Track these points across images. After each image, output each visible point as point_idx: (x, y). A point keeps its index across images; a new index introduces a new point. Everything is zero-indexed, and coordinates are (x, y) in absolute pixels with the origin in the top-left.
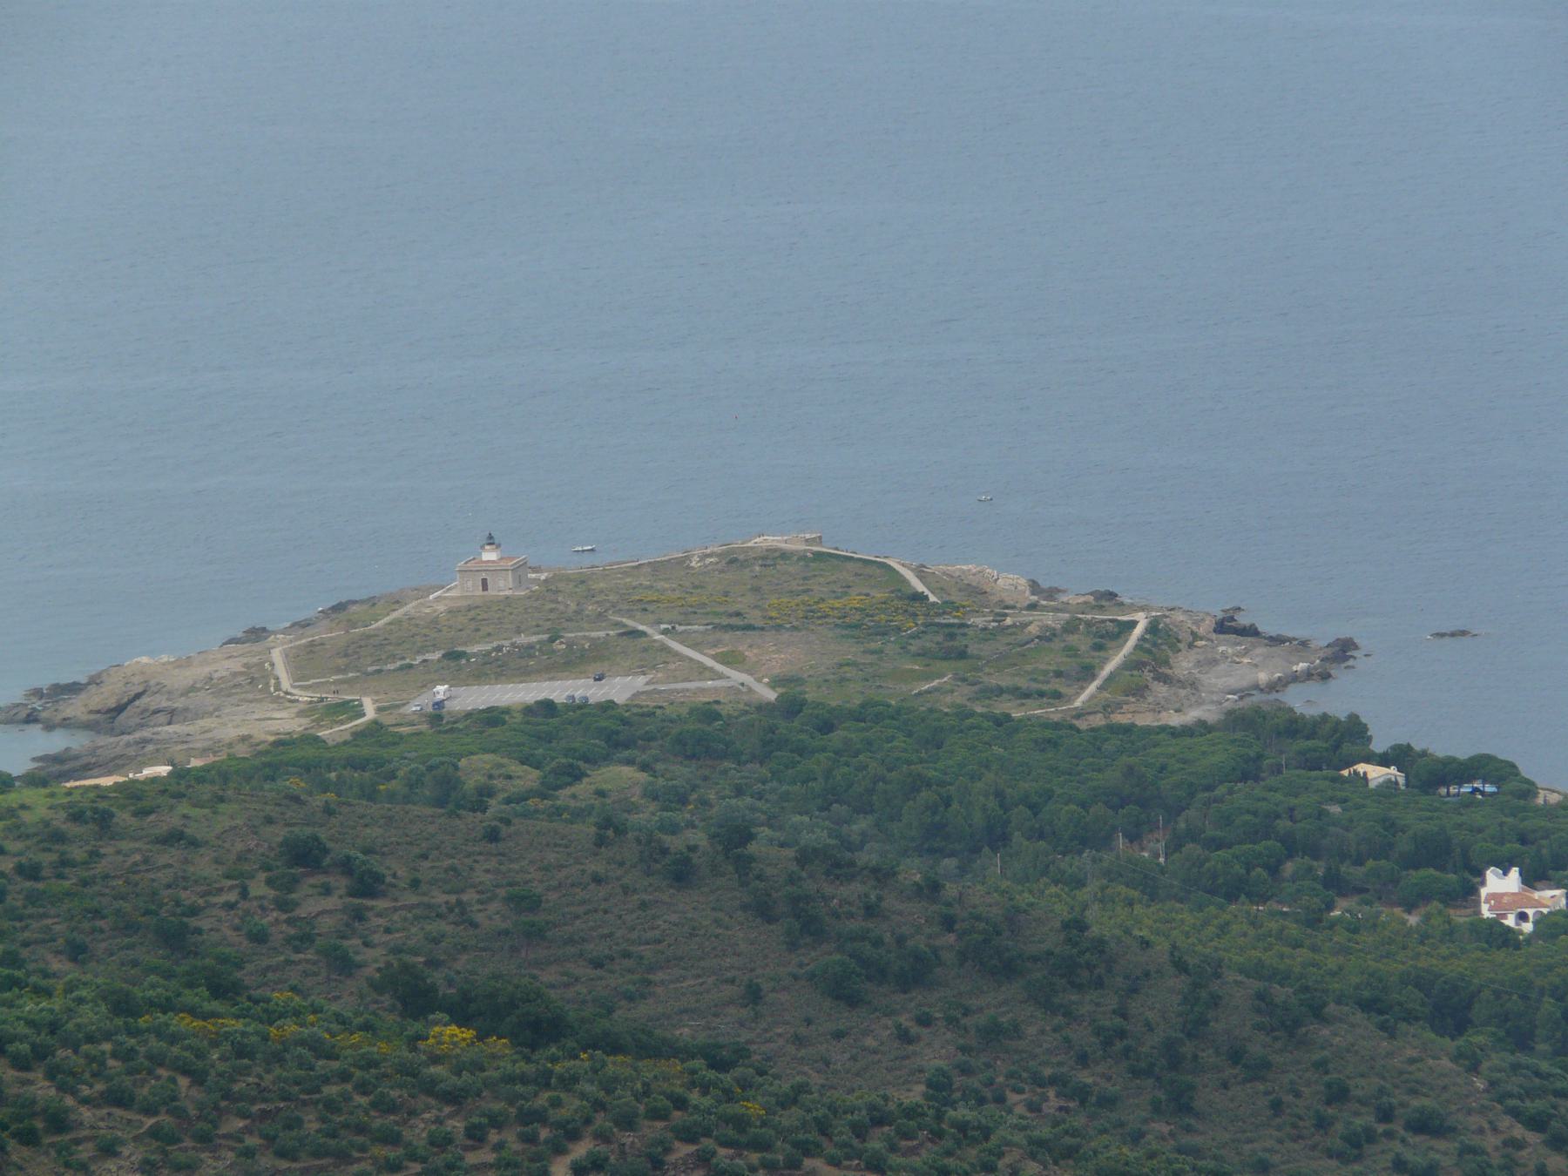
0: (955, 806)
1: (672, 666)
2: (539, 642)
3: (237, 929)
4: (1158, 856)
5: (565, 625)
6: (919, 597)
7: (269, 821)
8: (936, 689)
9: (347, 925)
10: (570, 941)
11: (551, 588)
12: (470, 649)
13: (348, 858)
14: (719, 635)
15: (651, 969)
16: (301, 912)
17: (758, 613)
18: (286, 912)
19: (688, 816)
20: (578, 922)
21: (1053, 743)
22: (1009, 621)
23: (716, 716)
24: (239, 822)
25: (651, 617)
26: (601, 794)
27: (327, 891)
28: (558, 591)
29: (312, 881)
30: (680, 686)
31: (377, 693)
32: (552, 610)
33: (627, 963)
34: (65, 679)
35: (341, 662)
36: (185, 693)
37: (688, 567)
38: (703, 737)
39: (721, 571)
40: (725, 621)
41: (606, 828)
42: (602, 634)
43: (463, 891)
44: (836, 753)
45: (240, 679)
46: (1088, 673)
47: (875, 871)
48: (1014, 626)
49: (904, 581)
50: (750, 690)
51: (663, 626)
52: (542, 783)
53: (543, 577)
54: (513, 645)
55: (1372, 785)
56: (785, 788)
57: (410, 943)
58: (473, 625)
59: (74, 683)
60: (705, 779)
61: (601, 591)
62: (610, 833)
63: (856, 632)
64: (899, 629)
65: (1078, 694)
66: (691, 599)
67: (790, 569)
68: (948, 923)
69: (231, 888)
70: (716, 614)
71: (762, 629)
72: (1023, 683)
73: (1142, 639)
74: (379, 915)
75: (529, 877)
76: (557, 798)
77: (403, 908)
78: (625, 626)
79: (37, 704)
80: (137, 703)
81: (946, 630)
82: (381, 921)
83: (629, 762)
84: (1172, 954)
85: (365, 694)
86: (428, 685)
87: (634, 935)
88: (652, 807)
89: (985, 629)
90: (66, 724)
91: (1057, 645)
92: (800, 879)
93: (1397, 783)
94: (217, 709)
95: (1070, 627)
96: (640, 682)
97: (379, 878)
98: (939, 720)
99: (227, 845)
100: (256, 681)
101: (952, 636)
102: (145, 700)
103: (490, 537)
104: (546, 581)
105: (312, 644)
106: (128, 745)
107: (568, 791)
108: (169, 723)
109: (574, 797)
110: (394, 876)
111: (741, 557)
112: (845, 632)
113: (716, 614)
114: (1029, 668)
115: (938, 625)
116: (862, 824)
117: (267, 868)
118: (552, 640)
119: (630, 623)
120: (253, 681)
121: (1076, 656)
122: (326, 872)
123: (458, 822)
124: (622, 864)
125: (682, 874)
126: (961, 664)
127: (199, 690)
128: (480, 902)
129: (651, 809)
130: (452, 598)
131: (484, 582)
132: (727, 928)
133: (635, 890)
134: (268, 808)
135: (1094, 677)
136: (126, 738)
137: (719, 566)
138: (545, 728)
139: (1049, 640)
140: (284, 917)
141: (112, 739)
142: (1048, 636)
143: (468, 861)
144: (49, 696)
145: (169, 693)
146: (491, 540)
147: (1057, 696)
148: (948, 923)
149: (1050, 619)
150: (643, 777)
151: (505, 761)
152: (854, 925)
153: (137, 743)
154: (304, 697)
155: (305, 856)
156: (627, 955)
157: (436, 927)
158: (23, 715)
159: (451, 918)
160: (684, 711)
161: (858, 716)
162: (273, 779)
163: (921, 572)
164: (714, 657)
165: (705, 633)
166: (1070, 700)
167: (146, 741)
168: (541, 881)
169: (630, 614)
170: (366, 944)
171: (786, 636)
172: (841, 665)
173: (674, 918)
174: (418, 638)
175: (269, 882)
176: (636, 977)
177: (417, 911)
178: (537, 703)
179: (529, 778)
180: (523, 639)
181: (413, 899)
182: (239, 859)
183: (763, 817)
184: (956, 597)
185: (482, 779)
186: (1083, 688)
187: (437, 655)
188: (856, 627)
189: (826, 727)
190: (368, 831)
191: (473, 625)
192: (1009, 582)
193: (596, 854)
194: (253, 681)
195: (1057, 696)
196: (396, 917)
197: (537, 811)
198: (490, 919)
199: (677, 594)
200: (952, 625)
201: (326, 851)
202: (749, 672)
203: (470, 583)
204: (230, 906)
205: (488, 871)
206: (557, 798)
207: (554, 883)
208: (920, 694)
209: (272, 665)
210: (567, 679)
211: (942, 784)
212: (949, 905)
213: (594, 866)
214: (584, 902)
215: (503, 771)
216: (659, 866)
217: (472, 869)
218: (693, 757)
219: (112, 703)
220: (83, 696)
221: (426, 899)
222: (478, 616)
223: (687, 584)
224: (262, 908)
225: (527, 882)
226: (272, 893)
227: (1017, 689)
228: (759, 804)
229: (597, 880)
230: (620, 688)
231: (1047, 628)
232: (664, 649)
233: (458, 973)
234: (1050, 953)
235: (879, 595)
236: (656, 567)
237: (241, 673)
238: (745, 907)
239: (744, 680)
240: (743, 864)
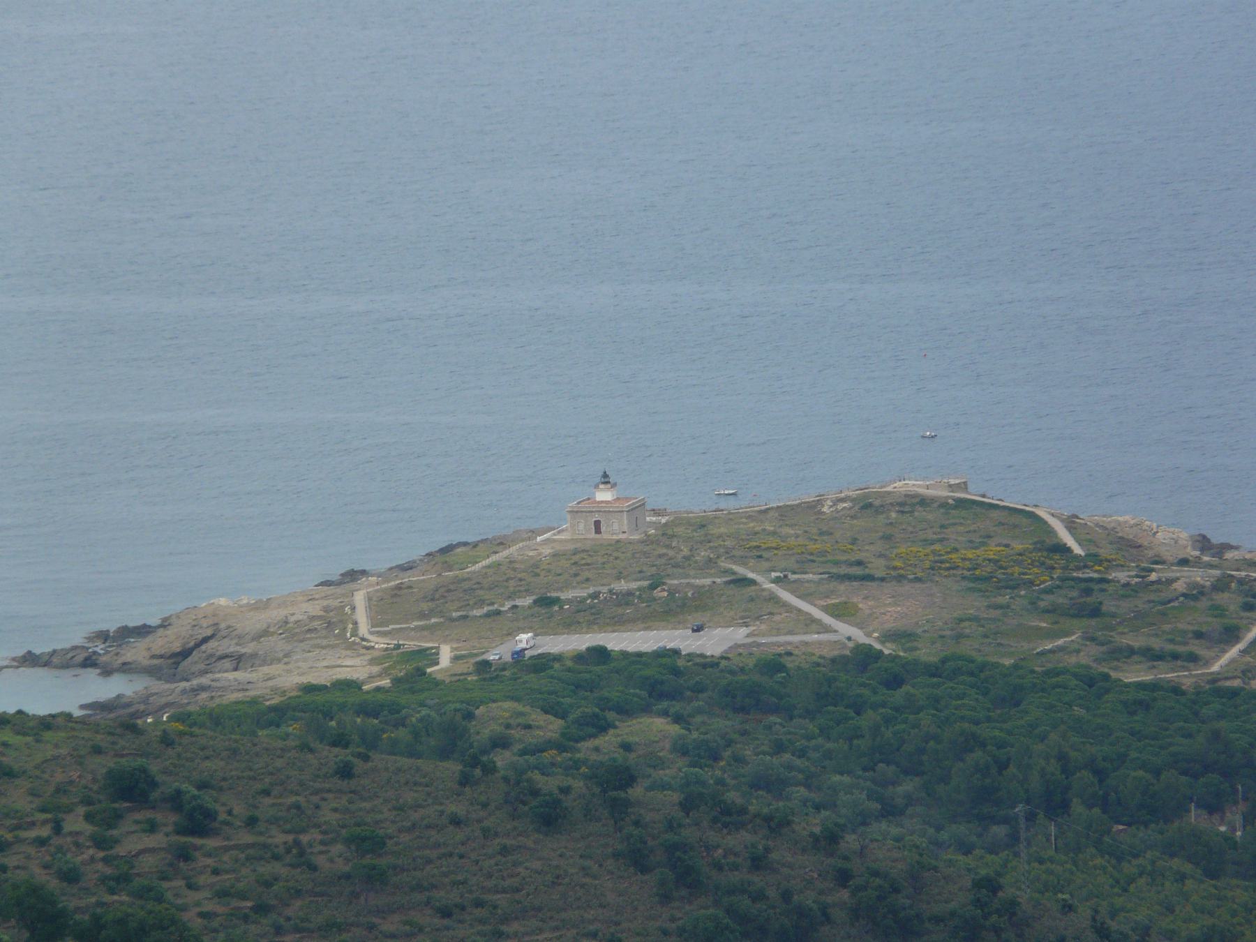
0: (1012, 769)
1: (777, 618)
2: (639, 589)
3: (46, 867)
4: (1234, 830)
5: (670, 571)
6: (1063, 549)
7: (97, 750)
8: (1061, 649)
9: (171, 865)
10: (419, 887)
11: (666, 534)
12: (563, 596)
13: (179, 793)
14: (833, 585)
15: (505, 920)
16: (121, 850)
17: (882, 562)
18: (103, 849)
19: (718, 773)
20: (428, 868)
21: (1145, 706)
22: (1153, 577)
23: (780, 668)
24: (63, 751)
25: (766, 565)
26: (627, 747)
27: (152, 828)
28: (673, 536)
29: (139, 816)
30: (782, 639)
31: (458, 641)
32: (660, 556)
33: (478, 912)
34: (133, 623)
35: (425, 606)
37: (821, 513)
38: (753, 690)
39: (852, 517)
40: (844, 570)
41: (474, 766)
42: (707, 581)
43: (303, 831)
44: (896, 709)
45: (316, 624)
46: (1231, 634)
47: (768, 819)
48: (1159, 582)
49: (1051, 532)
51: (774, 575)
52: (563, 735)
53: (663, 521)
54: (610, 591)
56: (830, 745)
57: (241, 886)
58: (574, 569)
59: (145, 626)
60: (744, 733)
61: (720, 536)
62: (478, 772)
63: (983, 586)
64: (1032, 583)
65: (1218, 657)
66: (812, 547)
67: (930, 517)
68: (843, 878)
69: (45, 822)
70: (837, 563)
71: (883, 579)
72: (1157, 644)
74: (209, 855)
75: (379, 817)
76: (579, 751)
77: (236, 847)
78: (734, 573)
79: (100, 648)
80: (203, 647)
81: (1083, 585)
82: (209, 861)
83: (665, 713)
84: (1094, 919)
85: (445, 642)
86: (511, 634)
87: (490, 884)
88: (681, 762)
89: (1128, 584)
90: (126, 668)
91: (1204, 603)
92: (680, 826)
94: (286, 656)
95: (1221, 585)
96: (740, 634)
97: (210, 815)
98: (1022, 677)
99: (46, 776)
100: (333, 626)
101: (1088, 592)
102: (212, 644)
103: (605, 475)
104: (666, 524)
105: (399, 587)
106: (184, 691)
107: (590, 744)
108: (236, 669)
109: (597, 749)
110: (230, 813)
111: (877, 503)
112: (972, 585)
113: (837, 563)
114: (1167, 627)
115: (1074, 579)
116: (908, 786)
117: (88, 802)
118: (653, 587)
119: (741, 570)
120: (330, 625)
121: (1222, 616)
122: (154, 808)
123: (310, 756)
124: (485, 805)
125: (551, 818)
126: (1093, 622)
127: (272, 634)
128: (322, 843)
129: (680, 764)
130: (561, 541)
131: (597, 524)
132: (595, 877)
133: (496, 834)
134: (99, 737)
135: (1237, 639)
136: (184, 684)
137: (852, 512)
138: (587, 676)
139: (1195, 598)
140: (101, 854)
141: (168, 686)
142: (1195, 593)
143: (315, 799)
144: (114, 639)
145: (239, 637)
146: (605, 479)
147: (1193, 658)
148: (843, 878)
149: (1199, 576)
150: (675, 729)
151: (528, 709)
152: (735, 878)
153: (193, 690)
154: (380, 643)
155: (131, 789)
156: (479, 904)
157: (266, 869)
158: (80, 658)
159: (288, 859)
160: (751, 663)
161: (933, 671)
162: (278, 726)
163: (1071, 523)
164: (826, 609)
165: (820, 582)
166: (1208, 663)
167: (203, 688)
168: (393, 822)
169: (743, 561)
170: (190, 887)
171: (907, 588)
172: (961, 620)
173: (537, 865)
174: (512, 583)
175: (89, 817)
176: (487, 928)
177: (251, 852)
178: (588, 649)
179: (552, 727)
180: (623, 586)
181: (247, 838)
182: (58, 790)
183: (800, 776)
184: (1105, 552)
185: (499, 729)
186: (1224, 651)
187: (529, 601)
188: (987, 579)
189: (894, 682)
190: (208, 764)
191: (574, 569)
192: (1170, 536)
193: (458, 795)
194: (330, 625)
195: (1193, 658)
196: (226, 858)
197: (553, 764)
198: (332, 861)
199: (801, 541)
200: (1091, 580)
201: (154, 784)
202: (860, 626)
203: (581, 526)
204: (41, 842)
205: (335, 810)
206: (579, 751)
207: (408, 824)
208: (1042, 653)
209: (353, 609)
210: (664, 628)
211: (1001, 745)
212: (846, 858)
213: (452, 808)
214: (437, 845)
215: (520, 720)
216: (526, 808)
217: (317, 807)
218: (742, 709)
219: (177, 647)
220: (149, 639)
221: (261, 839)
222: (580, 561)
223: (815, 530)
224: (77, 845)
225: (377, 822)
226: (89, 828)
227: (1149, 649)
228: (798, 762)
229: (456, 821)
230: (716, 641)
231: (1196, 585)
232: (773, 599)
233: (289, 919)
234: (953, 914)
235: (1018, 546)
236: (784, 512)
237: (319, 618)
238: (616, 855)
239: (824, 627)
240: (619, 808)
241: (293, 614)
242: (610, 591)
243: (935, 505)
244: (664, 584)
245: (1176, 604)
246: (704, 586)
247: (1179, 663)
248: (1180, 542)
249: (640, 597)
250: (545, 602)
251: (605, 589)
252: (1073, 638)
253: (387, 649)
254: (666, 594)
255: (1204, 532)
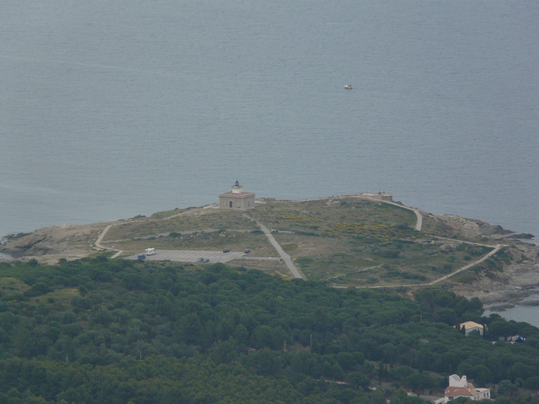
2: (214, 232)
12: (182, 233)
36: (58, 242)
39: (337, 208)
48: (434, 245)
50: (284, 263)
55: (467, 334)
73: (492, 257)
89: (421, 245)
93: (479, 332)
96: (238, 255)
102: (41, 243)
103: (237, 182)
118: (220, 232)
131: (231, 203)
135: (450, 272)
138: (76, 268)
139: (446, 253)
145: (52, 241)
146: (237, 185)
147: (423, 279)
166: (430, 281)
172: (336, 255)
186: (440, 277)
187: (167, 234)
203: (224, 203)
219: (26, 243)
241: (78, 233)
242: (202, 233)
243: (373, 205)
244: (225, 231)
245: (436, 255)
246: (241, 233)
247: (417, 280)
248: (474, 229)
249: (213, 236)
250: (174, 235)
251: (200, 231)
252: (379, 266)
253: (100, 251)
254: (224, 235)
255: (501, 225)
